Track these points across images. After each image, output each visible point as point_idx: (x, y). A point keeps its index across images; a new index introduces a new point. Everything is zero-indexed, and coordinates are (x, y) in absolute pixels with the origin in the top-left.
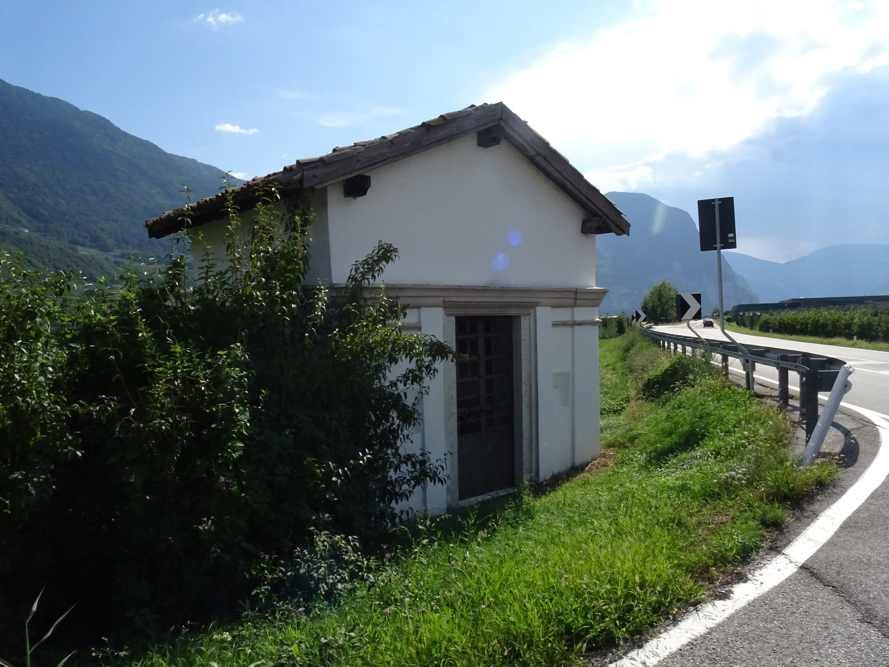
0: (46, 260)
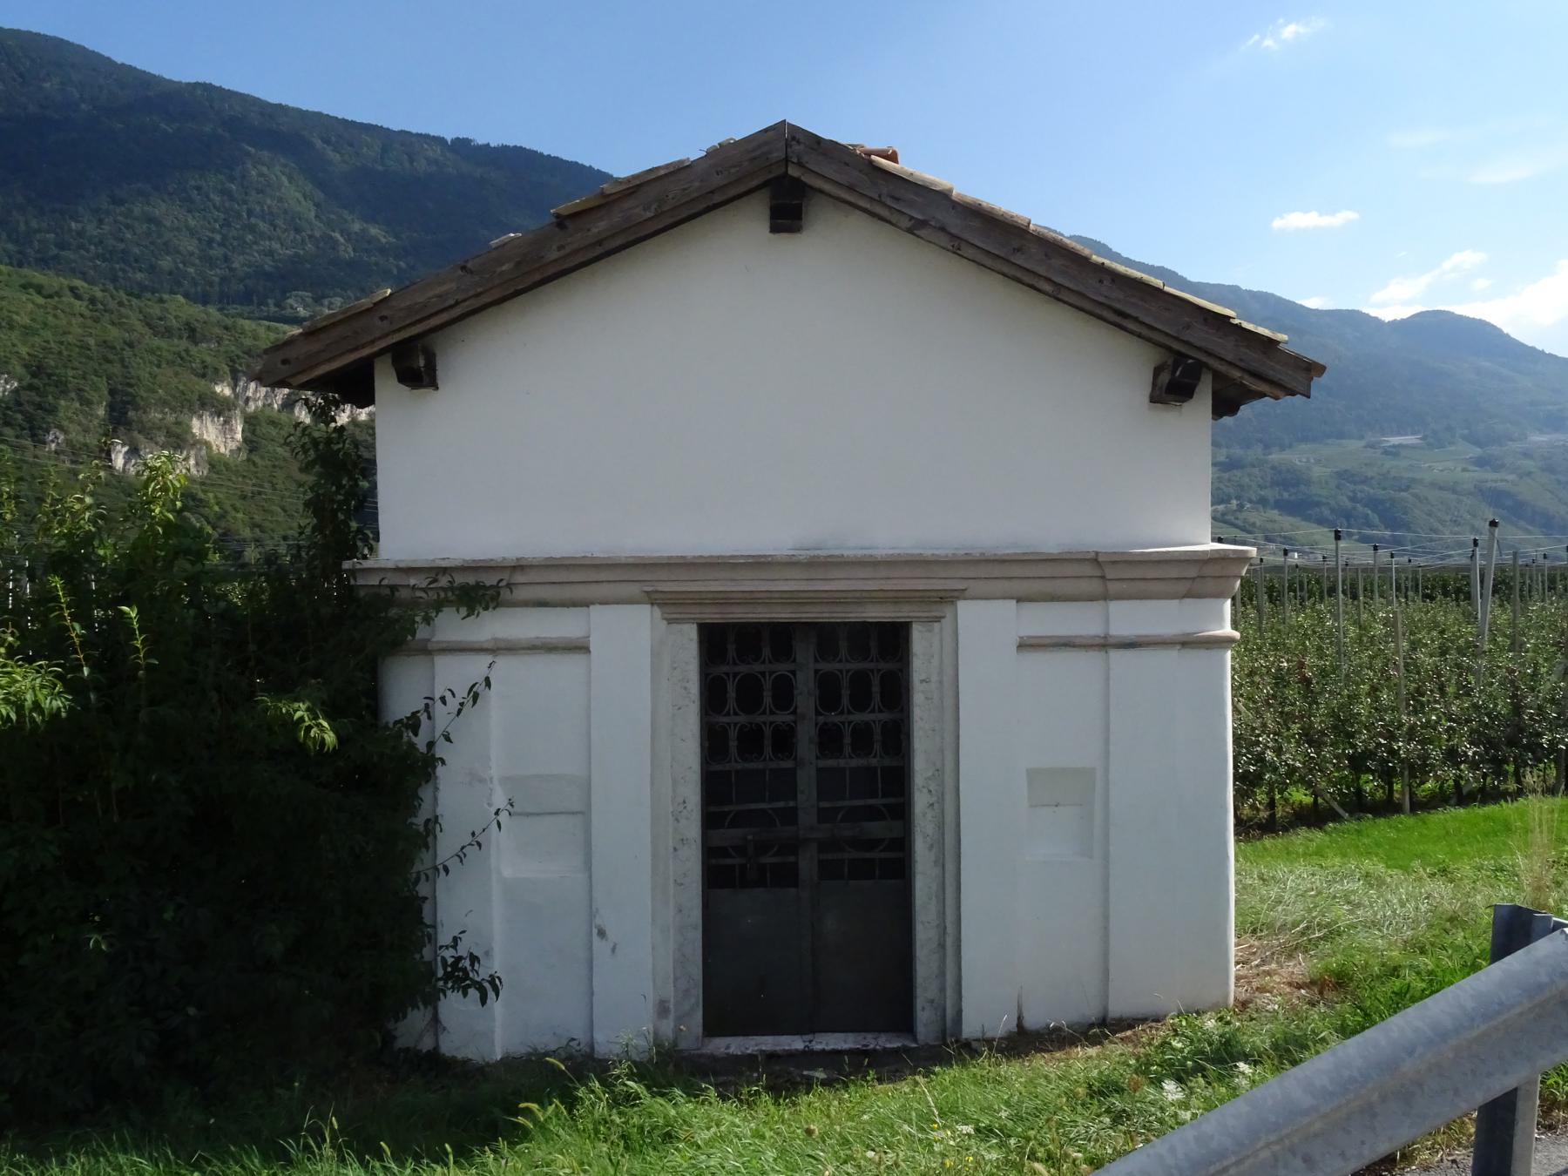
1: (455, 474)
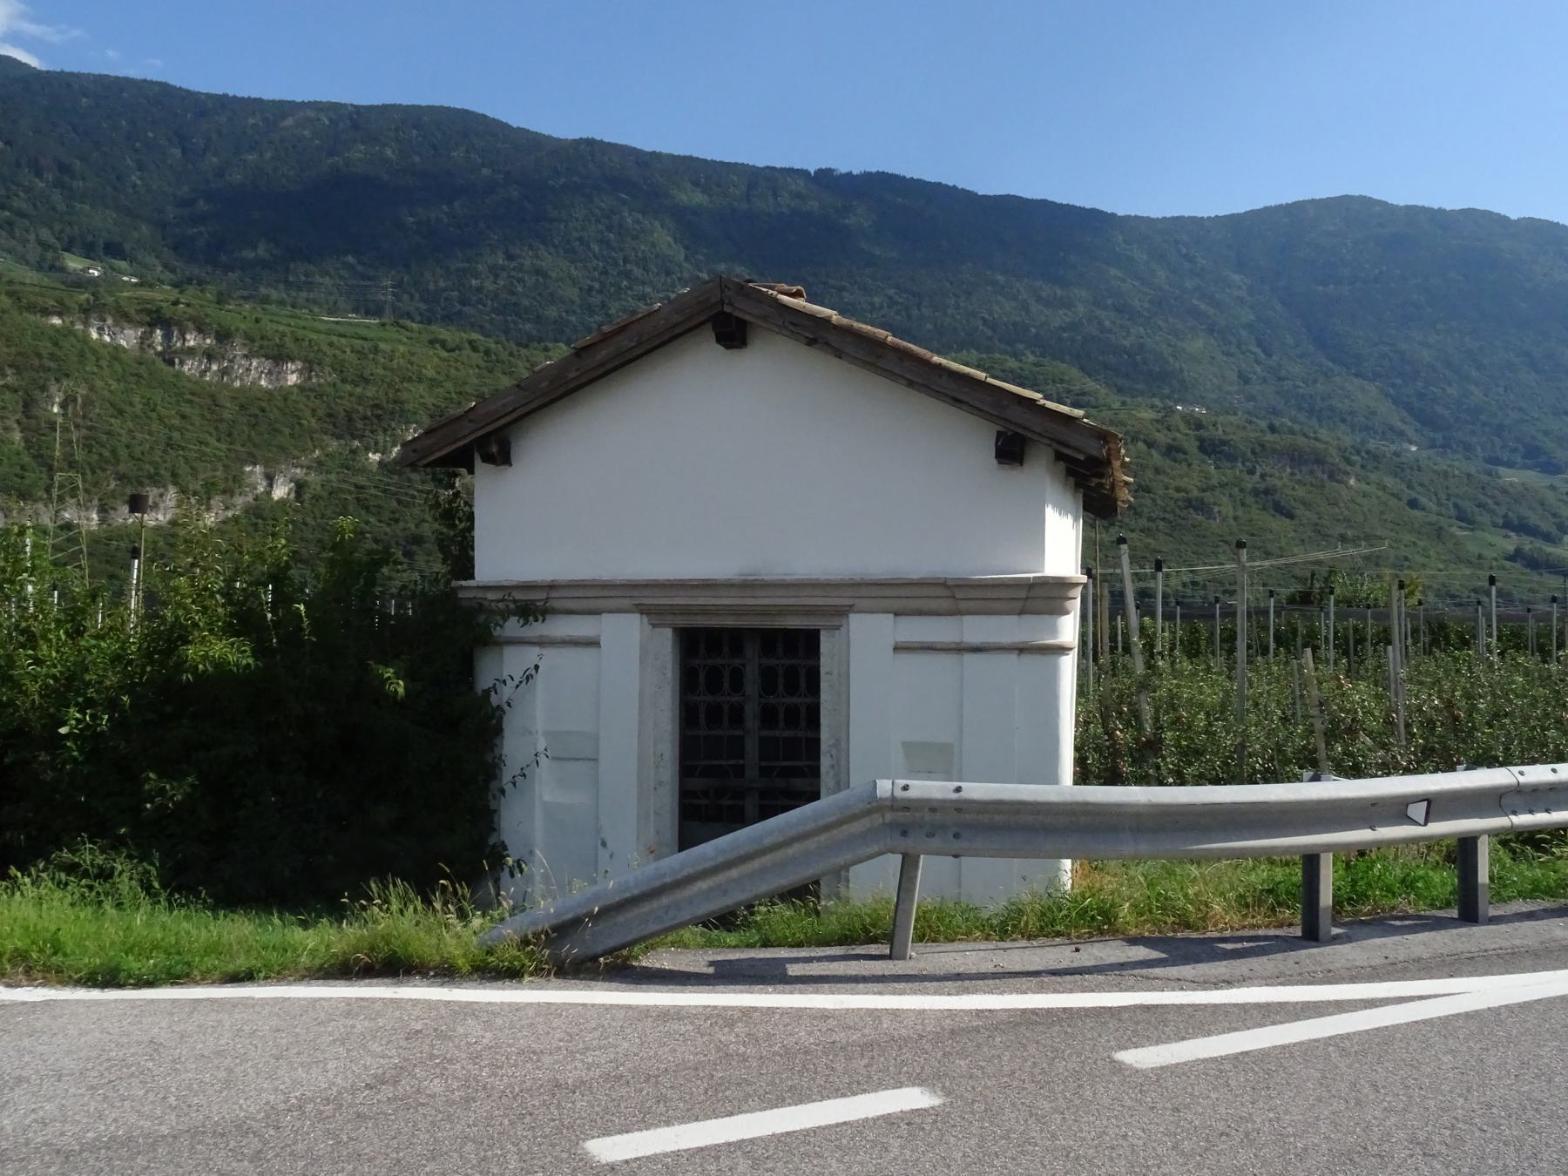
0: (1444, 497)
1: (523, 525)
